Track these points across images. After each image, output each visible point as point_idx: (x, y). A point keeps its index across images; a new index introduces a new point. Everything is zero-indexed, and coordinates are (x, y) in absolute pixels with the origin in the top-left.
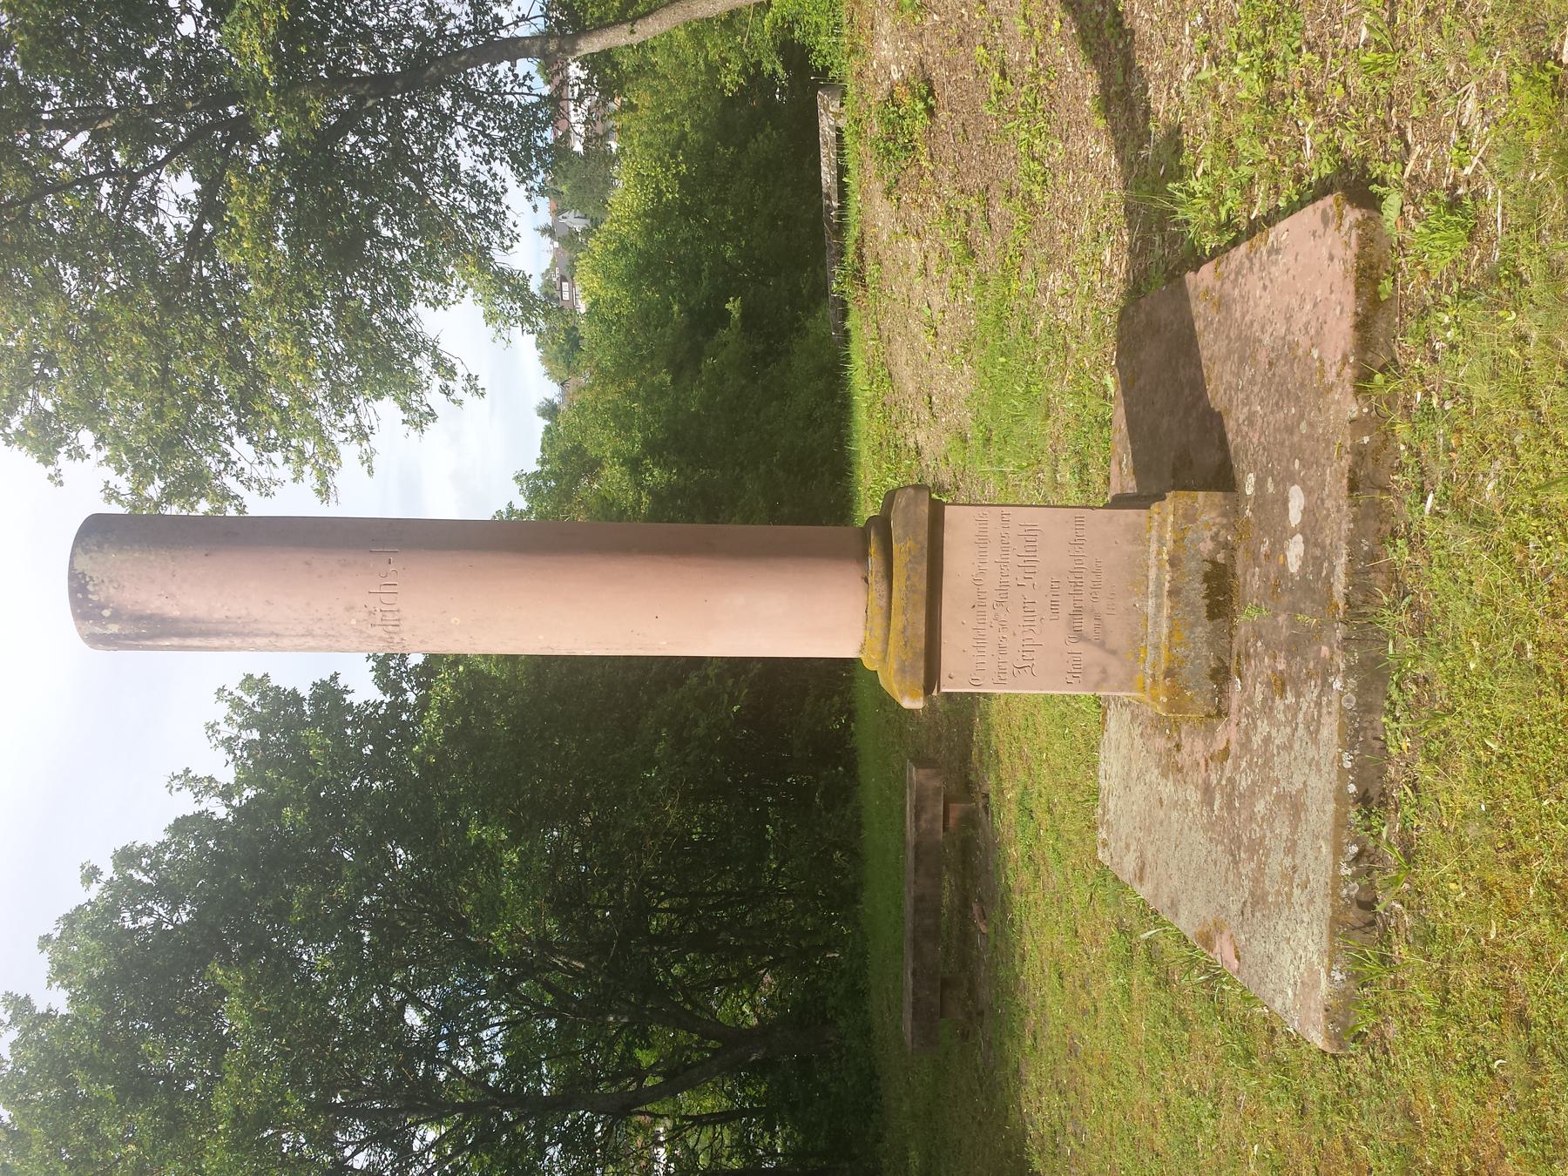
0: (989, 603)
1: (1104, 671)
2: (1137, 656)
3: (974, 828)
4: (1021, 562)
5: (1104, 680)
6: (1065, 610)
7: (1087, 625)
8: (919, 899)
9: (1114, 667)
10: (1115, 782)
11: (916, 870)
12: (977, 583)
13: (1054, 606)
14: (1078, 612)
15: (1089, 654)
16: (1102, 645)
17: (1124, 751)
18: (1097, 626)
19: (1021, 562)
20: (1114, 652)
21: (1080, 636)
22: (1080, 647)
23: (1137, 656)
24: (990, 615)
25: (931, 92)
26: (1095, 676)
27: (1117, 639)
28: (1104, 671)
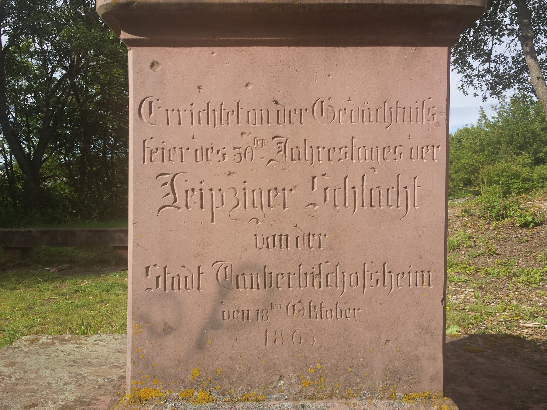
0: (283, 130)
1: (168, 330)
2: (194, 385)
3: (116, 265)
4: (354, 180)
5: (152, 331)
6: (274, 260)
7: (246, 298)
8: (73, 234)
9: (175, 348)
10: (86, 350)
11: (91, 231)
12: (318, 105)
13: (279, 240)
14: (269, 280)
15: (196, 305)
16: (213, 324)
17: (113, 358)
18: (245, 315)
19: (354, 180)
20: (200, 344)
21: (228, 285)
22: (209, 285)
23: (194, 385)
24: (263, 131)
25: (536, 224)
26: (159, 314)
27: (225, 349)
28: (168, 330)
